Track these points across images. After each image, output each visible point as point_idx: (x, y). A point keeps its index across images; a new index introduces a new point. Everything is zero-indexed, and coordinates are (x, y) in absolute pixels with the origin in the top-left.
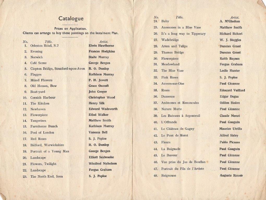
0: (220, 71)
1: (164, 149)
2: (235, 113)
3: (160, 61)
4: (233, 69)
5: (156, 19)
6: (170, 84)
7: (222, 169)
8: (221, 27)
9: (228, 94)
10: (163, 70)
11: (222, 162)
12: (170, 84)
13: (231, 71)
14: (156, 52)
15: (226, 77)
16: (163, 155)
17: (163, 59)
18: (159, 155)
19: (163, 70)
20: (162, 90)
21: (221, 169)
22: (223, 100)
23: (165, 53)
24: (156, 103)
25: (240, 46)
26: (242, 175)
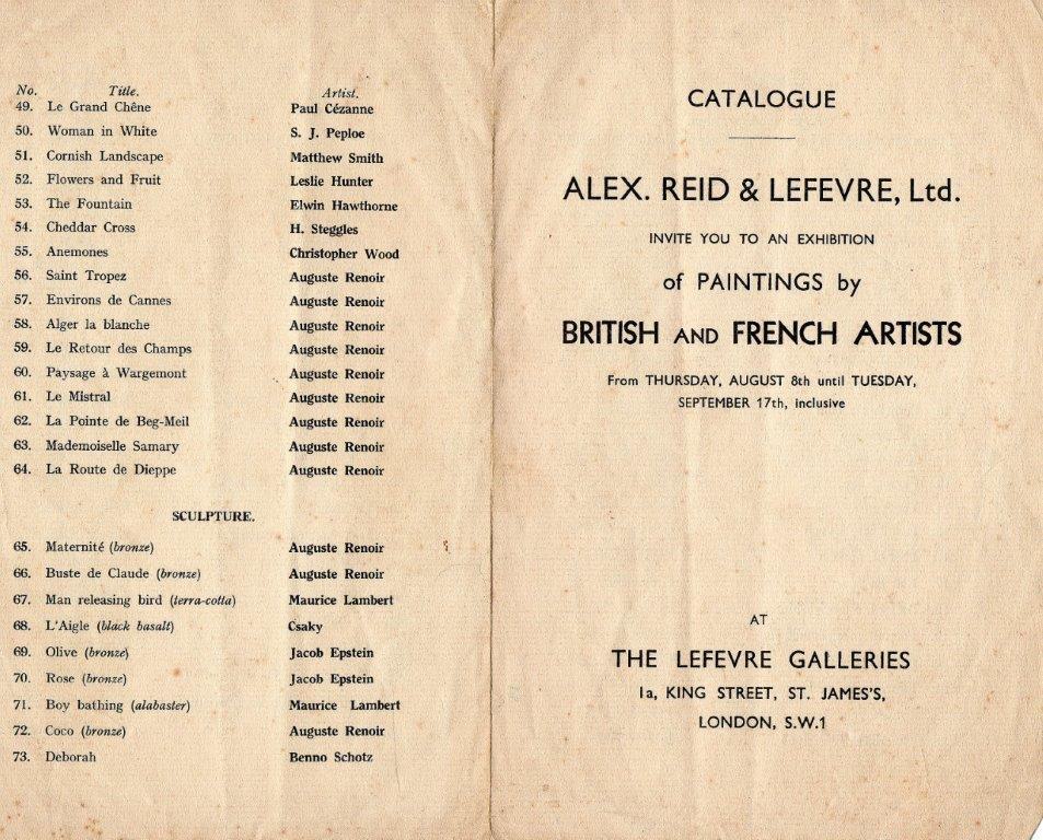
0: (293, 184)
1: (59, 471)
2: (362, 339)
3: (39, 168)
4: (345, 177)
5: (24, 98)
6: (87, 181)
7: (299, 109)
8: (297, 157)
9: (325, 171)
10: (55, 203)
11: (299, 109)
12: (87, 181)
13: (336, 183)
14: (22, 251)
15: (316, 133)
16: (52, 348)
17: (54, 182)
18: (37, 420)
19: (55, 203)
20: (50, 678)
21: (298, 111)
22: (301, 193)
23: (61, 181)
24: (22, 599)
25: (379, 375)
26: (382, 350)
